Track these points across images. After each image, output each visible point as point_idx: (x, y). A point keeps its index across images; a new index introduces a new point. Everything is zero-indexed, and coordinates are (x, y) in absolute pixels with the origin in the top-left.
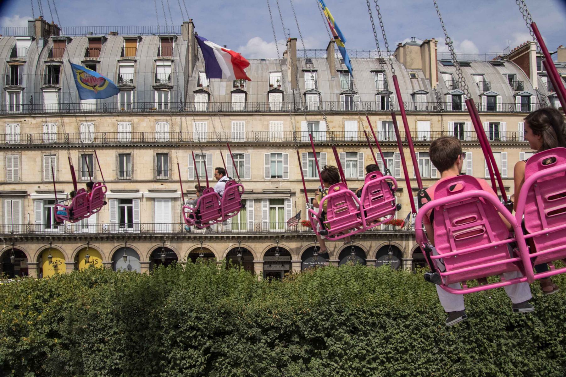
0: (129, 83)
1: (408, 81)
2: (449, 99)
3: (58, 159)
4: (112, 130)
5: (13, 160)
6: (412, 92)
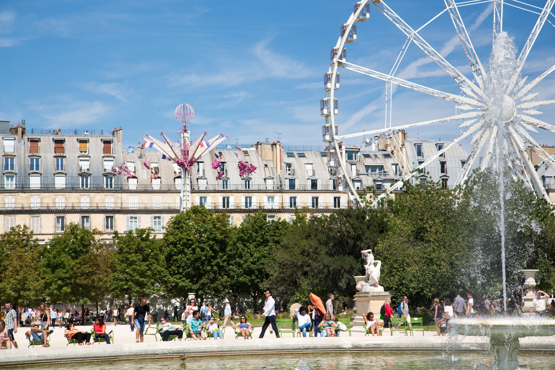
0: (86, 171)
1: (263, 169)
2: (287, 182)
3: (41, 219)
4: (77, 201)
5: (10, 220)
6: (264, 177)
